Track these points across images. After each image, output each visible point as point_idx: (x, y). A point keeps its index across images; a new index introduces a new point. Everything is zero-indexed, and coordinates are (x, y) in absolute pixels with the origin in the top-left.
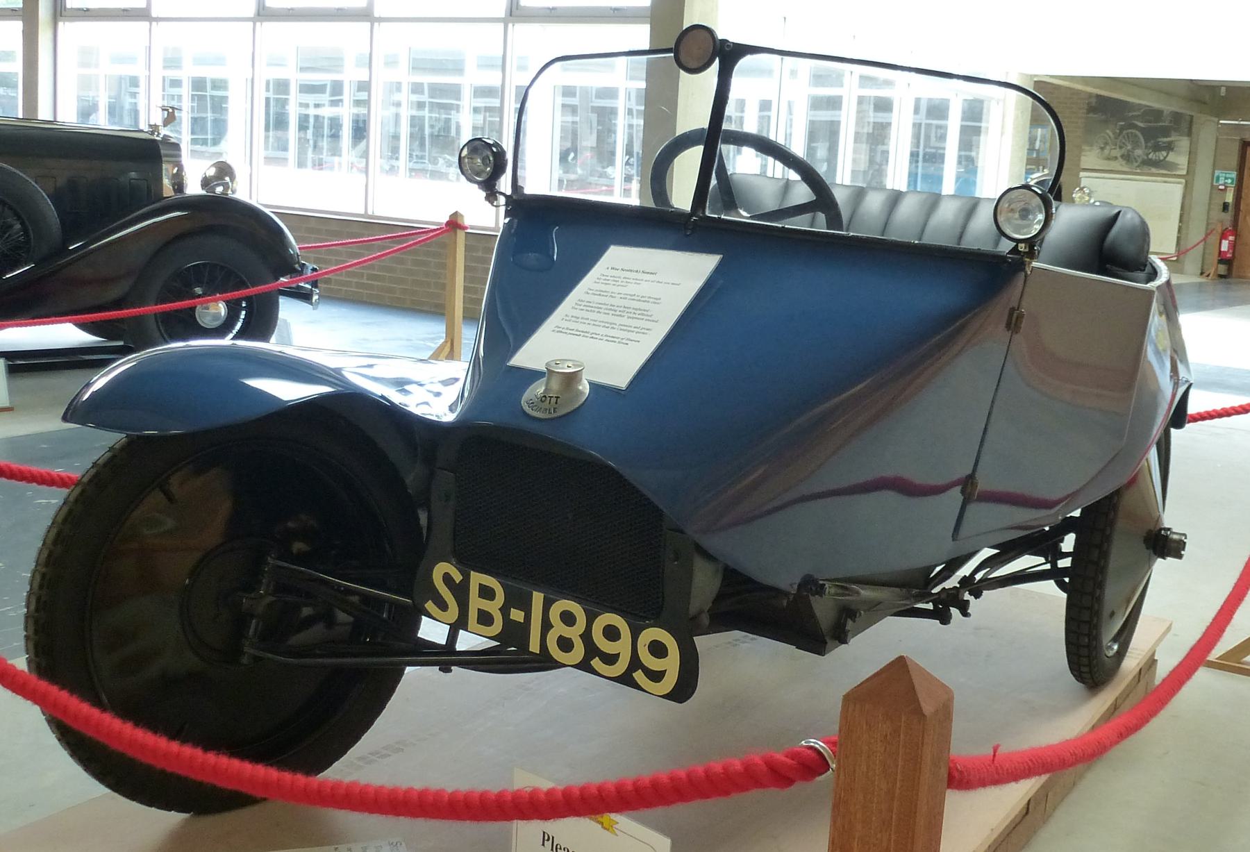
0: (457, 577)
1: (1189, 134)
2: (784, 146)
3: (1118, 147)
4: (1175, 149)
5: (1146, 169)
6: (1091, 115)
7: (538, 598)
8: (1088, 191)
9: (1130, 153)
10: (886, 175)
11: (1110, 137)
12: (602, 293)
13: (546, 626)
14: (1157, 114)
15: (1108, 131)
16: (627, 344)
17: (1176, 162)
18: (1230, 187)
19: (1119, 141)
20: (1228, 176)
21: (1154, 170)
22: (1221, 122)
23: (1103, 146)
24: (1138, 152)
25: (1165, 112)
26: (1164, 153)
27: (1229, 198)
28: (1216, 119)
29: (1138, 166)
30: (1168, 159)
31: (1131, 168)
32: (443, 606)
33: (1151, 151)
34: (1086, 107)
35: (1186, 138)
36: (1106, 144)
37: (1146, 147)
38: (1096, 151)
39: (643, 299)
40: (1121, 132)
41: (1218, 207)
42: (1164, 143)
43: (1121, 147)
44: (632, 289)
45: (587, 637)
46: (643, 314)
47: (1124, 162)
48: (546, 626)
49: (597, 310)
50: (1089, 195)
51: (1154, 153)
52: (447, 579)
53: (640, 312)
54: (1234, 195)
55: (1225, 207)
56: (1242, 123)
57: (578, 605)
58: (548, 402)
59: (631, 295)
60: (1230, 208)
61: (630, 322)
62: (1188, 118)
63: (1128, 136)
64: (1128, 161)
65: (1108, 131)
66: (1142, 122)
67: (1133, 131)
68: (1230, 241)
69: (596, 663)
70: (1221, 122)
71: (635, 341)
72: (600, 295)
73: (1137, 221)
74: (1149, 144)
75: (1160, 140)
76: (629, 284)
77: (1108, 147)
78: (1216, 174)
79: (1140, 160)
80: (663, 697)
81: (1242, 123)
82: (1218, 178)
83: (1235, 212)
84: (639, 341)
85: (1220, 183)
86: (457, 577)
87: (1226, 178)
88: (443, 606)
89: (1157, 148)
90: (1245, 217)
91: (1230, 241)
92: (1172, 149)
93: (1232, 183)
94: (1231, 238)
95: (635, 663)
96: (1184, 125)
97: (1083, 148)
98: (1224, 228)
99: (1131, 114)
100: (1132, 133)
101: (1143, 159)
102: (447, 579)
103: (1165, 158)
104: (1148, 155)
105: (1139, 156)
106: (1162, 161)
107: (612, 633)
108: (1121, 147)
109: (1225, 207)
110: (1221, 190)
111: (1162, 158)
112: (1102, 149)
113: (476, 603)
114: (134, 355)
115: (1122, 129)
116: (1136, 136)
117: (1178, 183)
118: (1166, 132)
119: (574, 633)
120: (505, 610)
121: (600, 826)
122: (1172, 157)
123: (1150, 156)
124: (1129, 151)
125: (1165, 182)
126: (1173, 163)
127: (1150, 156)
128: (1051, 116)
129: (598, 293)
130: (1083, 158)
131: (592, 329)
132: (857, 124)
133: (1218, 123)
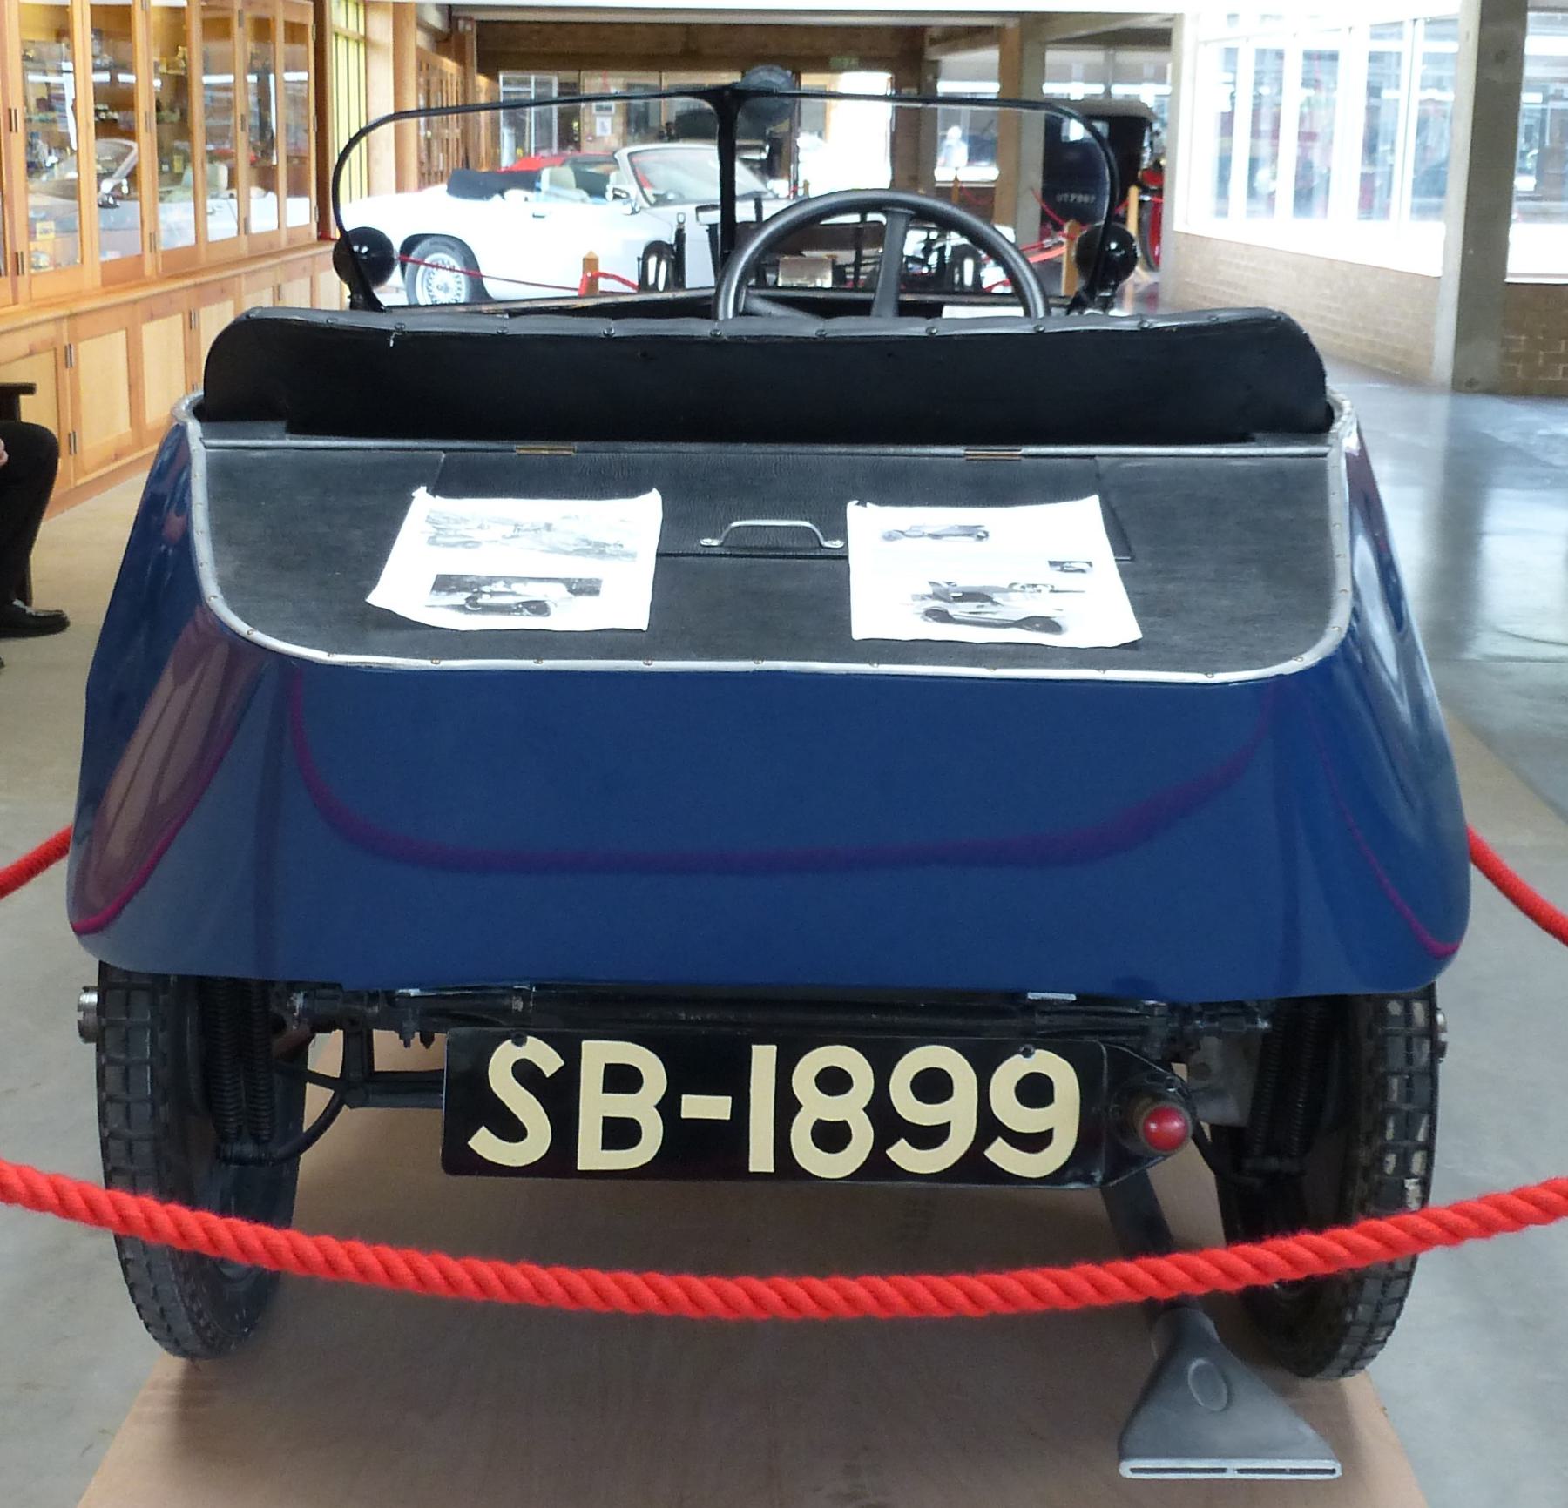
0: (548, 1060)
2: (312, 310)
7: (764, 1058)
10: (1127, 96)
13: (786, 1106)
45: (880, 1109)
48: (786, 1106)
52: (526, 1073)
86: (548, 1060)
89: (636, 122)
95: (989, 1127)
96: (1321, 67)
102: (526, 1073)
107: (933, 1086)
113: (595, 1105)
114: (844, 449)
117: (1527, 104)
119: (851, 1108)
120: (668, 1107)
128: (1017, 106)
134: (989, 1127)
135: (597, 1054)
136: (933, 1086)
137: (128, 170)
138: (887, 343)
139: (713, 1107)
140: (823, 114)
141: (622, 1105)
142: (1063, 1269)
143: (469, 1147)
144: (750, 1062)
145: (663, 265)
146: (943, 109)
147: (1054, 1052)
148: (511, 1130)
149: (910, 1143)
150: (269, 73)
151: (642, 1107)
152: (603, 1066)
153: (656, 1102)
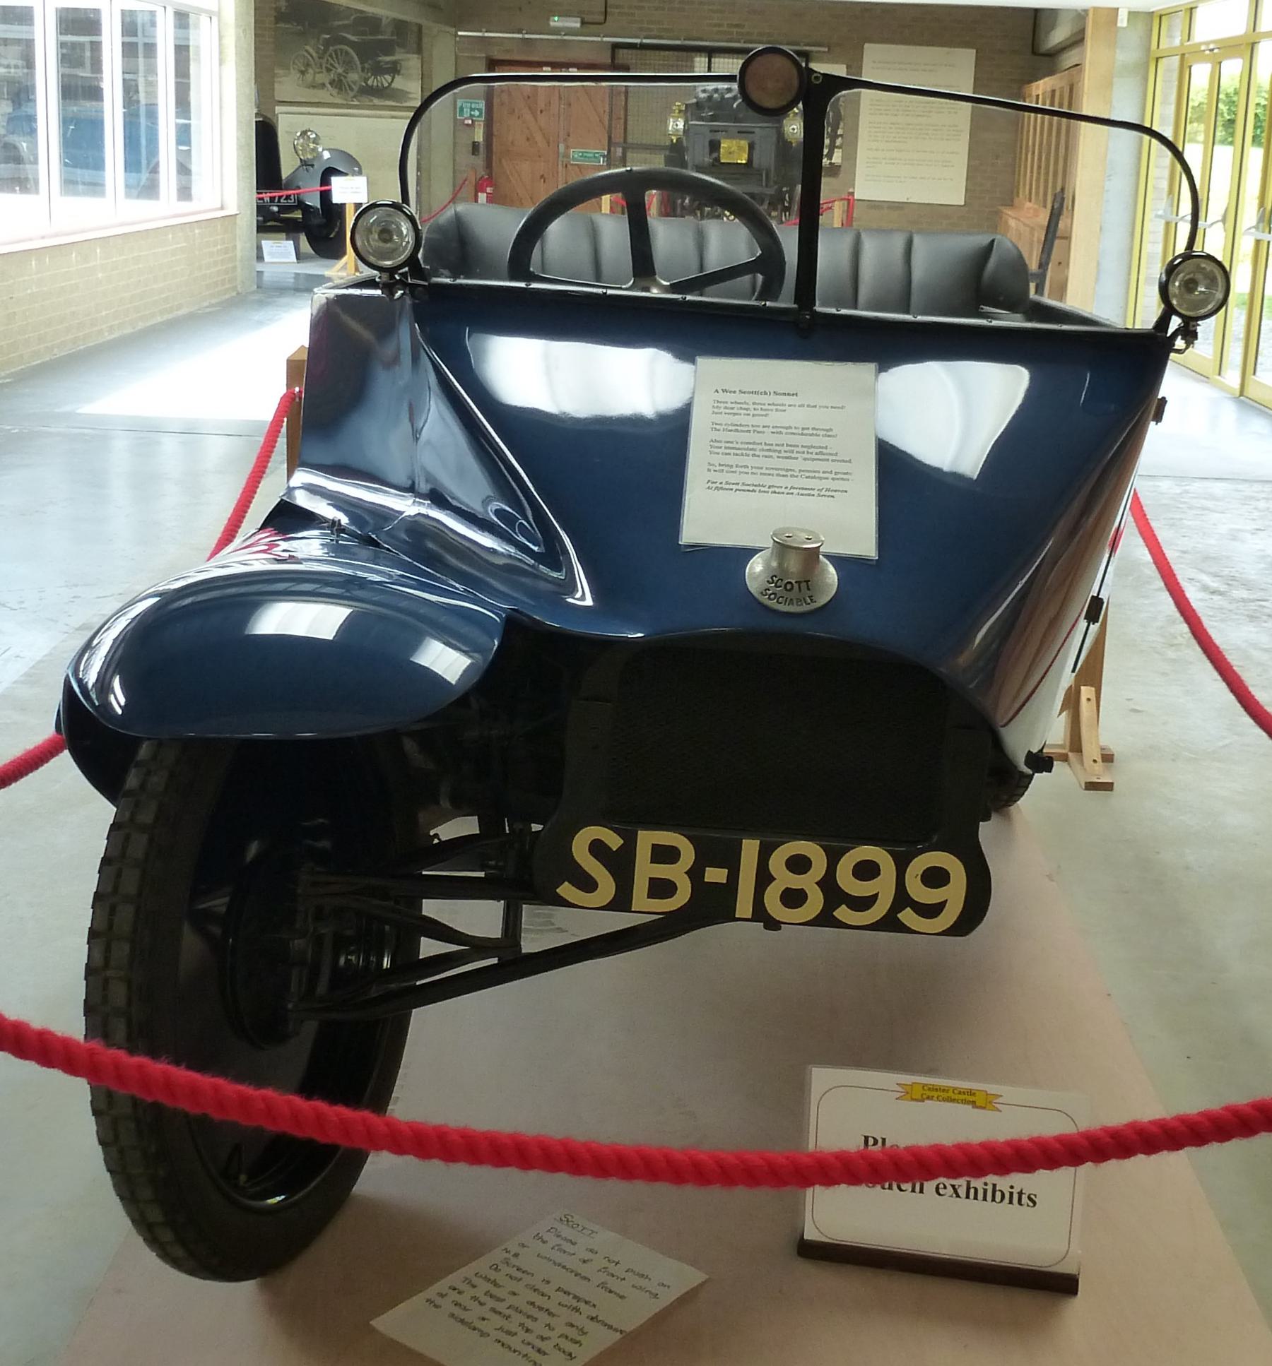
0: (614, 841)
1: (419, 50)
3: (324, 70)
4: (402, 72)
5: (366, 100)
6: (281, 25)
7: (750, 848)
8: (314, 136)
9: (342, 78)
11: (311, 56)
12: (739, 428)
13: (764, 878)
14: (372, 23)
15: (308, 48)
16: (833, 497)
17: (405, 89)
18: (478, 121)
19: (324, 61)
20: (473, 106)
21: (376, 101)
22: (460, 33)
23: (303, 69)
24: (354, 76)
25: (384, 22)
26: (389, 78)
27: (479, 136)
28: (453, 30)
29: (355, 97)
30: (393, 85)
31: (346, 100)
32: (588, 884)
33: (370, 74)
34: (273, 13)
35: (416, 56)
36: (308, 65)
37: (363, 70)
38: (295, 75)
39: (805, 432)
40: (325, 51)
41: (465, 150)
42: (387, 63)
43: (328, 70)
44: (775, 418)
45: (828, 884)
46: (821, 453)
47: (335, 92)
48: (764, 878)
49: (752, 452)
50: (315, 141)
51: (376, 78)
52: (597, 848)
53: (818, 450)
54: (484, 133)
55: (475, 146)
56: (486, 34)
57: (810, 843)
58: (797, 590)
59: (787, 428)
60: (482, 149)
61: (810, 465)
62: (415, 29)
63: (336, 54)
64: (341, 89)
65: (308, 48)
66: (353, 35)
67: (346, 48)
68: (488, 194)
69: (843, 913)
70: (460, 33)
71: (842, 491)
72: (737, 431)
73: (1015, 252)
74: (366, 65)
75: (380, 58)
76: (770, 412)
77: (311, 71)
78: (459, 104)
79: (356, 88)
80: (945, 933)
81: (486, 34)
82: (462, 109)
83: (488, 152)
84: (846, 492)
85: (465, 116)
86: (614, 841)
87: (472, 109)
88: (588, 884)
89: (378, 70)
90: (500, 161)
91: (488, 194)
92: (398, 72)
93: (480, 116)
94: (489, 190)
97: (276, 72)
98: (478, 177)
99: (337, 23)
100: (341, 50)
101: (361, 85)
102: (597, 848)
103: (390, 84)
104: (366, 80)
105: (355, 83)
106: (386, 88)
108: (328, 70)
109: (475, 146)
110: (468, 125)
111: (386, 85)
112: (303, 73)
113: (645, 870)
115: (327, 43)
116: (347, 53)
118: (387, 48)
119: (808, 882)
120: (695, 874)
121: (970, 1107)
122: (399, 83)
123: (370, 82)
124: (340, 75)
125: (393, 117)
126: (403, 91)
127: (370, 82)
129: (733, 428)
130: (276, 86)
131: (768, 481)
132: (177, 76)
133: (456, 35)
134: (902, 899)
135: (647, 839)
136: (866, 871)
137: (1038, 265)
138: (536, 292)
139: (716, 875)
140: (857, 100)
141: (663, 871)
142: (240, 1083)
146: (1031, 103)
147: (955, 856)
151: (677, 873)
152: (650, 848)
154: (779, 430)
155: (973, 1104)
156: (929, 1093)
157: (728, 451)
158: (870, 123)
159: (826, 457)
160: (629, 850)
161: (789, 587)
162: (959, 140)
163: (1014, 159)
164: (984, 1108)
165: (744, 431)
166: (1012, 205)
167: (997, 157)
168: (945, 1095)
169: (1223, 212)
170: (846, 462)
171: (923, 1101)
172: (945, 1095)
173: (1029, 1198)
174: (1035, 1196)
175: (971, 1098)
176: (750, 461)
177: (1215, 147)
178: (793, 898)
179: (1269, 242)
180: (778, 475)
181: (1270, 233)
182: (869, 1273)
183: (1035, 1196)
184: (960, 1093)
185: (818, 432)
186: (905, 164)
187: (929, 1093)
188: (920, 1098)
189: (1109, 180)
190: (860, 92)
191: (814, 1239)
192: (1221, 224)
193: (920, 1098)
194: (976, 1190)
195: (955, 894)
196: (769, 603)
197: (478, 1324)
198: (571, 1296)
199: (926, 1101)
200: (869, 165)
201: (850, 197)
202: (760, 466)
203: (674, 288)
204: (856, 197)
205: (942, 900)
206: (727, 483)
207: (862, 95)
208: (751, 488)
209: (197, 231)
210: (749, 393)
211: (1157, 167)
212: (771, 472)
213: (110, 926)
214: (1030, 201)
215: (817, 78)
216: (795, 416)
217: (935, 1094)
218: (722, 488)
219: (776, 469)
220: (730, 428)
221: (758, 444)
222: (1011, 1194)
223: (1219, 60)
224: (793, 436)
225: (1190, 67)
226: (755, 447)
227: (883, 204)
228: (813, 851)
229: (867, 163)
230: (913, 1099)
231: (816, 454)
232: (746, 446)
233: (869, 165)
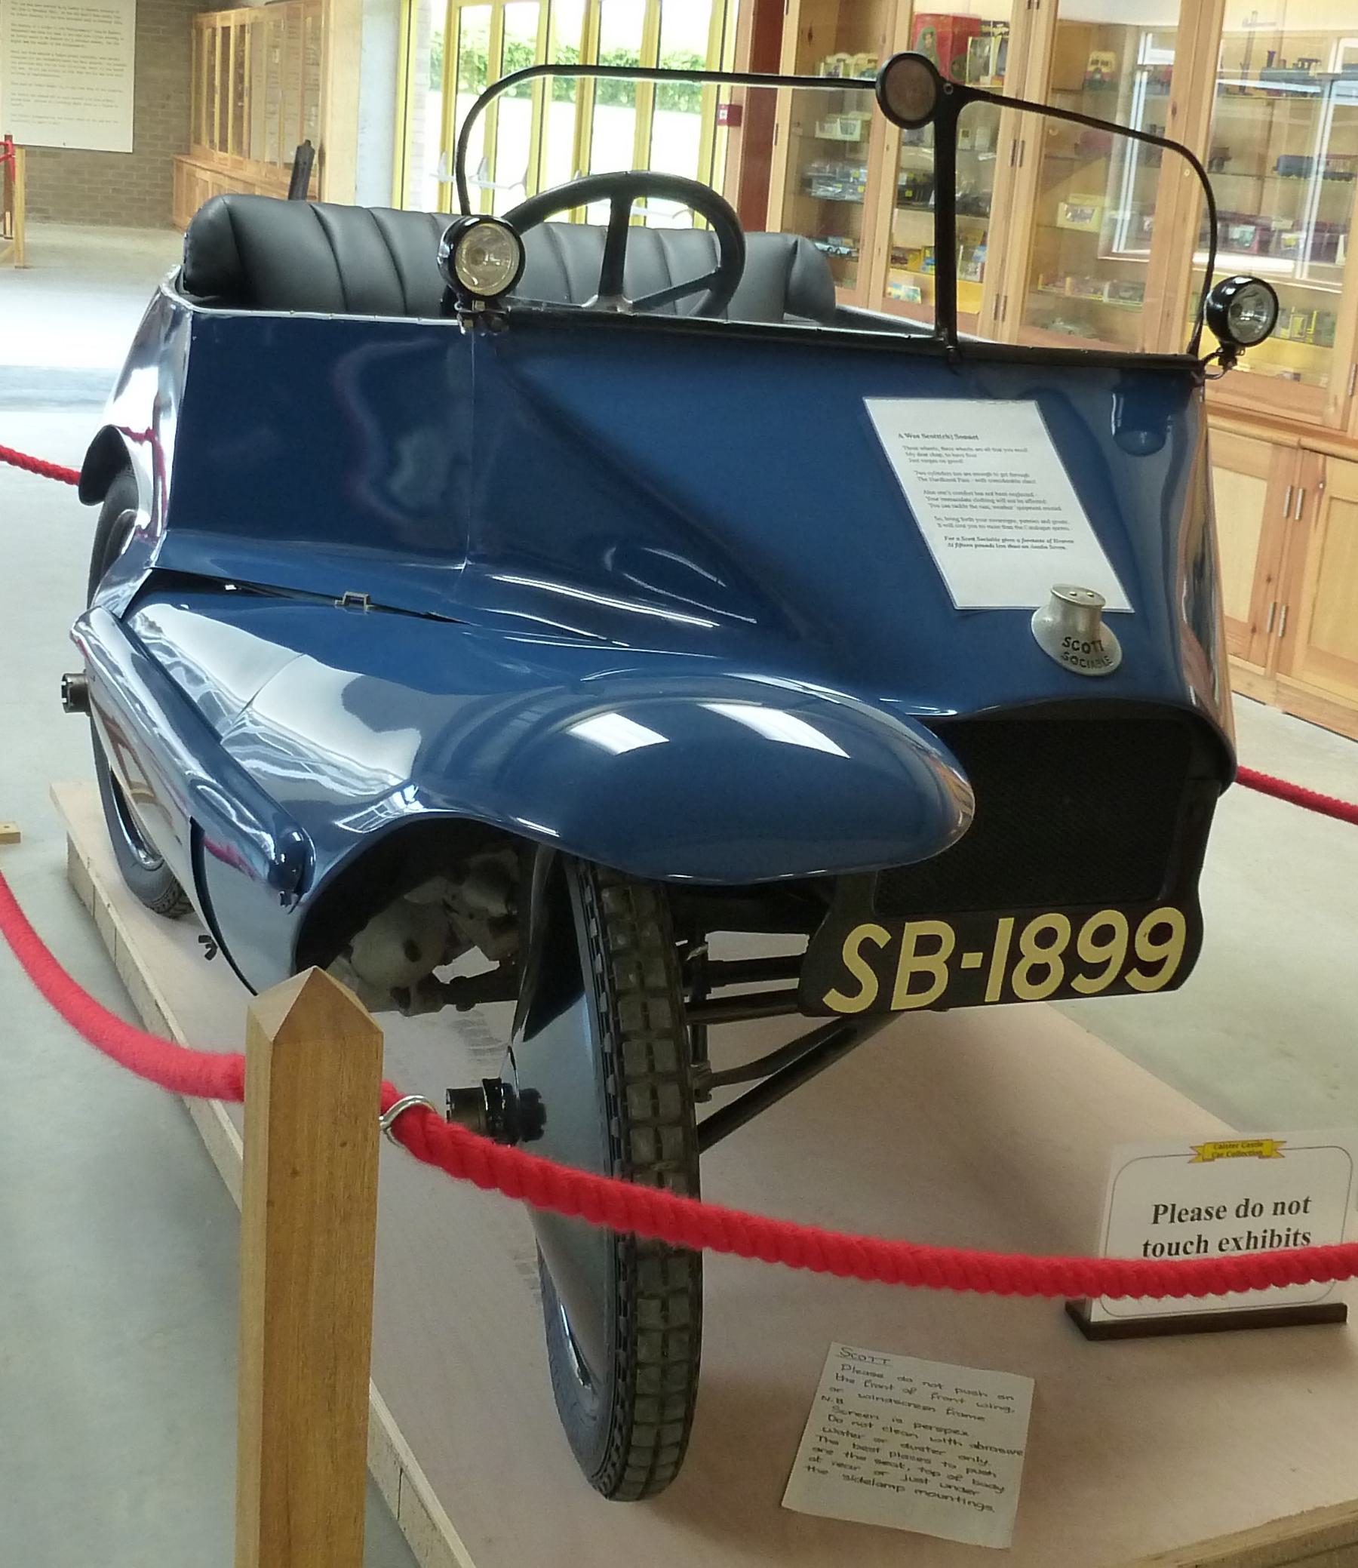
0: (881, 936)
7: (1005, 926)
13: (1015, 955)
44: (969, 465)
48: (1015, 955)
52: (867, 949)
72: (942, 480)
86: (881, 936)
102: (867, 949)
113: (909, 963)
119: (1052, 956)
120: (953, 963)
121: (1257, 1158)
134: (1132, 960)
135: (913, 930)
136: (1103, 936)
139: (972, 960)
143: (824, 1003)
144: (1200, 911)
145: (1122, 400)
148: (852, 987)
149: (838, 991)
150: (1339, 233)
153: (1060, 952)
154: (981, 477)
155: (1260, 1155)
156: (1220, 1151)
157: (947, 503)
158: (13, 51)
159: (1038, 505)
160: (895, 945)
161: (1086, 648)
162: (121, 76)
163: (189, 100)
164: (1268, 1157)
165: (948, 480)
166: (189, 154)
167: (168, 97)
168: (1234, 1150)
169: (524, 172)
170: (1056, 509)
171: (1212, 1160)
172: (1234, 1150)
173: (1304, 1238)
174: (1309, 1234)
175: (1259, 1149)
176: (967, 513)
177: (656, 112)
178: (1038, 974)
179: (645, 217)
180: (1004, 527)
181: (646, 206)
182: (1166, 1341)
183: (1309, 1234)
184: (1248, 1146)
185: (1018, 478)
186: (59, 102)
187: (1220, 1151)
188: (1210, 1157)
189: (363, 133)
190: (776, 89)
191: (1101, 1320)
192: (522, 187)
193: (1210, 1157)
194: (1256, 1238)
195: (1173, 949)
196: (1074, 668)
197: (879, 1479)
198: (934, 1429)
199: (1216, 1160)
200: (14, 102)
201: (8, 142)
202: (984, 518)
203: (637, 306)
204: (14, 142)
205: (1162, 957)
206: (1024, 541)
207: (779, 91)
208: (988, 543)
209: (1260, 327)
210: (934, 437)
211: (415, 119)
212: (997, 524)
213: (655, 1110)
214: (223, 147)
215: (949, 88)
216: (985, 462)
217: (1224, 1151)
218: (961, 545)
219: (1000, 521)
220: (936, 477)
221: (970, 494)
222: (1288, 1236)
223: (459, 5)
224: (995, 483)
225: (460, 9)
226: (968, 497)
227: (37, 149)
228: (1059, 922)
229: (12, 100)
230: (1204, 1160)
231: (1027, 502)
232: (960, 497)
233: (14, 102)
